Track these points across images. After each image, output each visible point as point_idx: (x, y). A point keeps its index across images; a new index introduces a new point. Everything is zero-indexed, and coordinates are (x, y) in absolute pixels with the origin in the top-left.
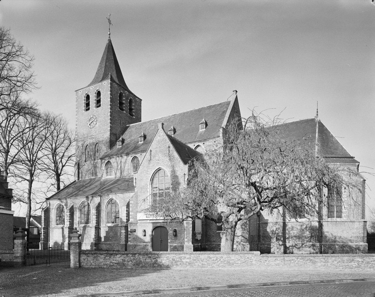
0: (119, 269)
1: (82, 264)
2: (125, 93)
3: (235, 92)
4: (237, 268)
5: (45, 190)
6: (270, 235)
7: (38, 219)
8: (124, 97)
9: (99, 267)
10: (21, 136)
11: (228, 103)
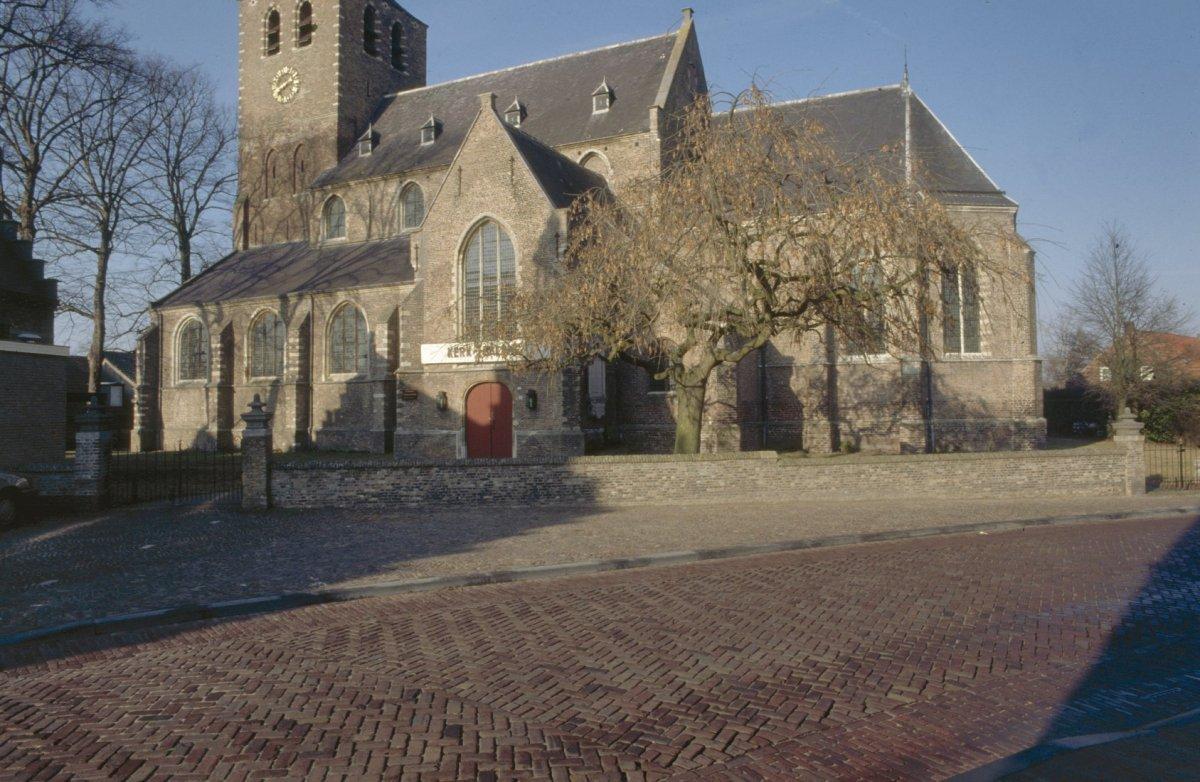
0: (385, 511)
1: (277, 498)
2: (381, 9)
3: (688, 12)
4: (715, 501)
5: (144, 277)
6: (341, 296)
7: (125, 360)
8: (378, 19)
9: (326, 507)
10: (75, 123)
11: (670, 43)
